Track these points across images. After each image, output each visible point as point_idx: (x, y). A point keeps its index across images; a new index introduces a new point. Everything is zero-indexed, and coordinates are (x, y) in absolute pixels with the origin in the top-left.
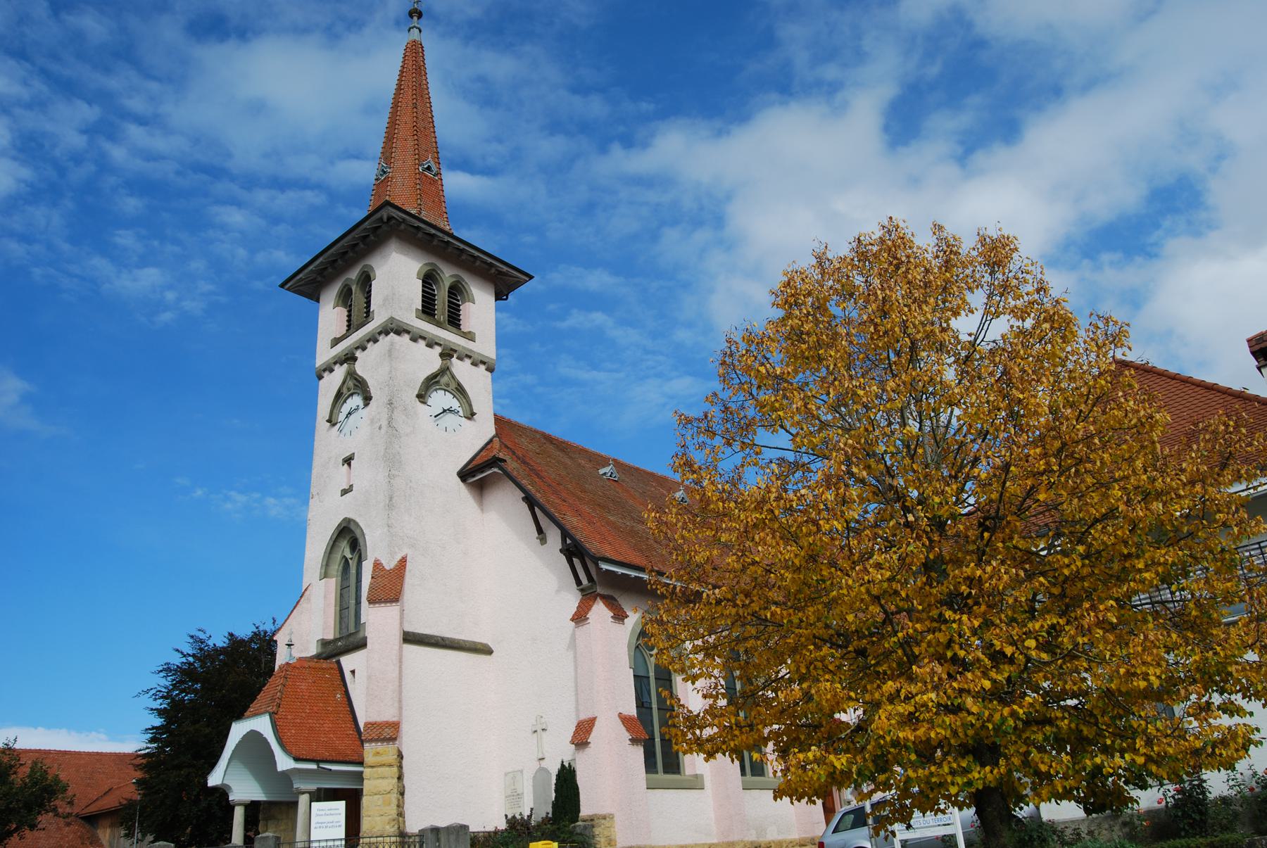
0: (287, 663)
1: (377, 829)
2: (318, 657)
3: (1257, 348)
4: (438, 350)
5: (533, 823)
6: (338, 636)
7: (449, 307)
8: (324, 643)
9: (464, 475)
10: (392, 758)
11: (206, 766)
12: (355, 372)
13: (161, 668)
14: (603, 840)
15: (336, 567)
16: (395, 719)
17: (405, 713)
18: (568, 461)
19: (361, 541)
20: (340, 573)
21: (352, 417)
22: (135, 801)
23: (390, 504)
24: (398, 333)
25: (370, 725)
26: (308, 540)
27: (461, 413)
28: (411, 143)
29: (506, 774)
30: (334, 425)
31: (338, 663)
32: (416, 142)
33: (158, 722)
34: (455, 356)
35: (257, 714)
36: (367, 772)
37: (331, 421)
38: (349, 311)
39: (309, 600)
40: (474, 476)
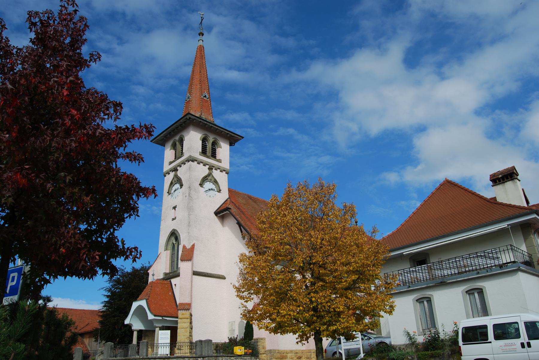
0: (152, 281)
1: (182, 341)
2: (163, 279)
3: (492, 179)
4: (208, 166)
5: (238, 340)
6: (170, 272)
7: (212, 150)
8: (166, 274)
9: (216, 213)
10: (188, 316)
11: (124, 316)
12: (177, 175)
13: (108, 280)
14: (261, 347)
15: (170, 247)
16: (189, 302)
17: (193, 300)
18: (256, 206)
19: (179, 238)
20: (171, 249)
21: (176, 192)
22: (99, 328)
23: (189, 225)
24: (193, 161)
25: (181, 304)
26: (160, 236)
27: (216, 190)
28: (198, 86)
29: (229, 323)
30: (170, 194)
31: (170, 281)
32: (201, 86)
33: (107, 300)
34: (214, 168)
35: (141, 299)
36: (179, 320)
37: (169, 193)
38: (176, 151)
39: (160, 258)
40: (220, 214)
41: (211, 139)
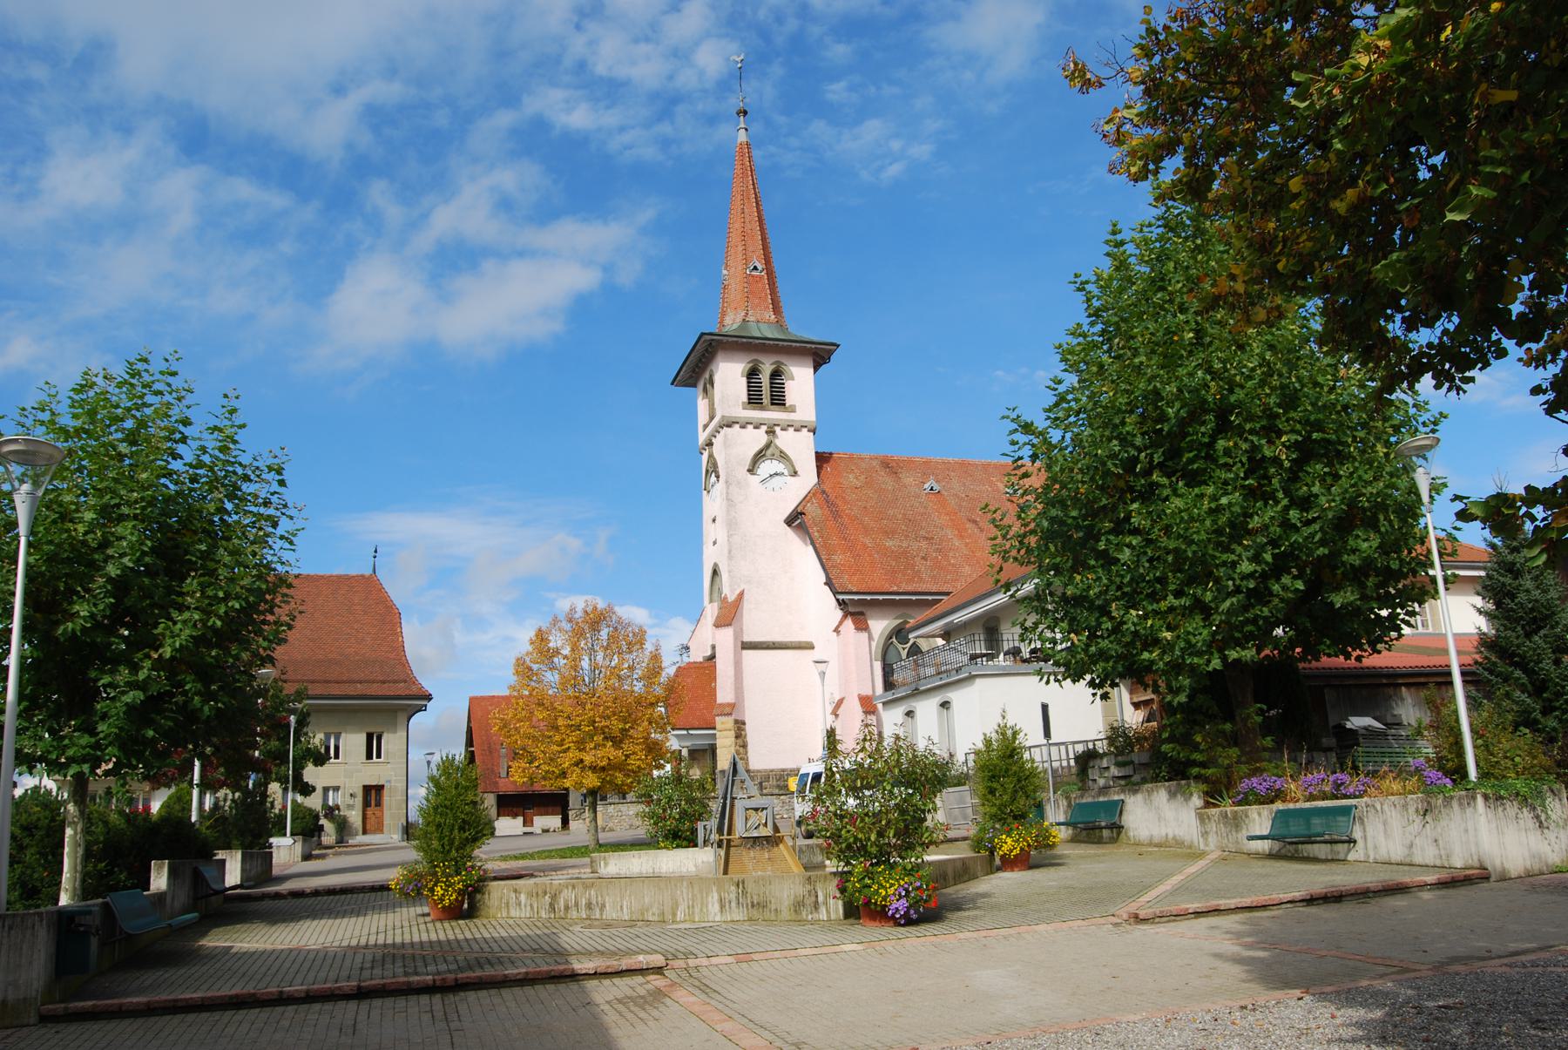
4: (764, 428)
24: (729, 426)
27: (786, 473)
28: (740, 248)
36: (718, 734)
41: (767, 369)
